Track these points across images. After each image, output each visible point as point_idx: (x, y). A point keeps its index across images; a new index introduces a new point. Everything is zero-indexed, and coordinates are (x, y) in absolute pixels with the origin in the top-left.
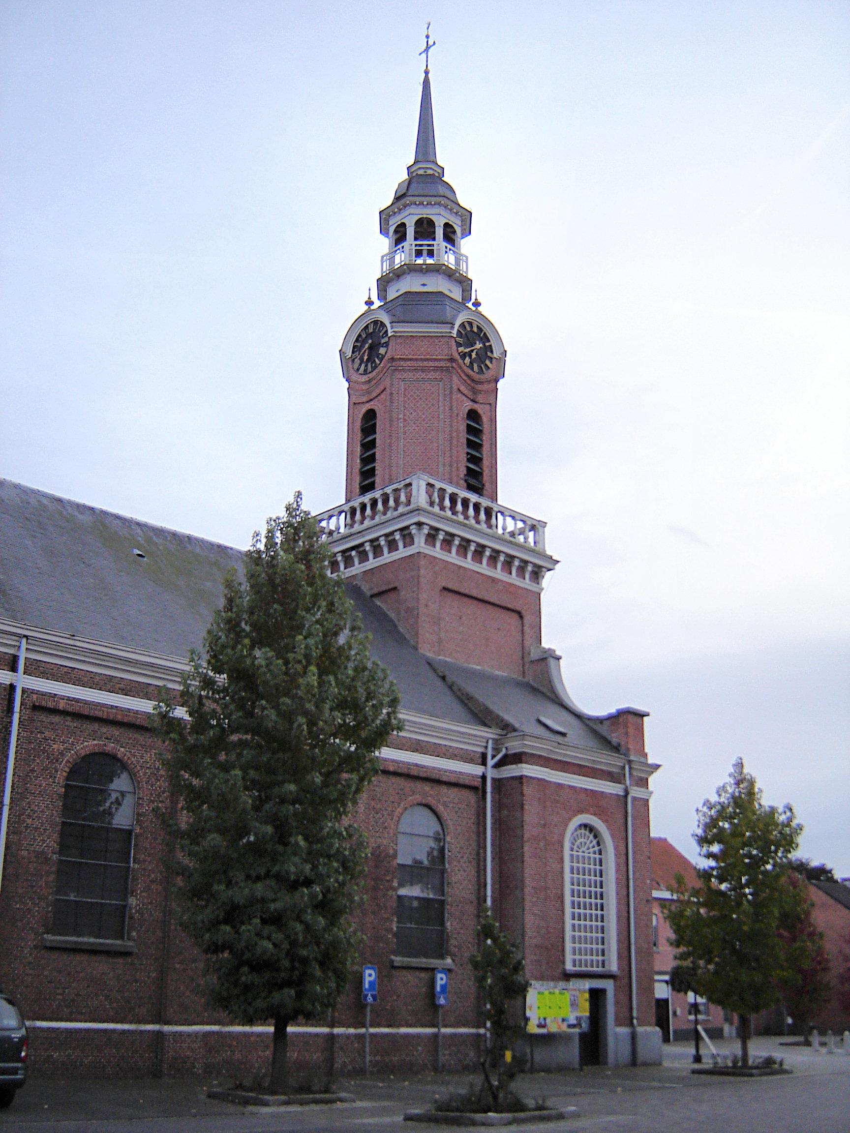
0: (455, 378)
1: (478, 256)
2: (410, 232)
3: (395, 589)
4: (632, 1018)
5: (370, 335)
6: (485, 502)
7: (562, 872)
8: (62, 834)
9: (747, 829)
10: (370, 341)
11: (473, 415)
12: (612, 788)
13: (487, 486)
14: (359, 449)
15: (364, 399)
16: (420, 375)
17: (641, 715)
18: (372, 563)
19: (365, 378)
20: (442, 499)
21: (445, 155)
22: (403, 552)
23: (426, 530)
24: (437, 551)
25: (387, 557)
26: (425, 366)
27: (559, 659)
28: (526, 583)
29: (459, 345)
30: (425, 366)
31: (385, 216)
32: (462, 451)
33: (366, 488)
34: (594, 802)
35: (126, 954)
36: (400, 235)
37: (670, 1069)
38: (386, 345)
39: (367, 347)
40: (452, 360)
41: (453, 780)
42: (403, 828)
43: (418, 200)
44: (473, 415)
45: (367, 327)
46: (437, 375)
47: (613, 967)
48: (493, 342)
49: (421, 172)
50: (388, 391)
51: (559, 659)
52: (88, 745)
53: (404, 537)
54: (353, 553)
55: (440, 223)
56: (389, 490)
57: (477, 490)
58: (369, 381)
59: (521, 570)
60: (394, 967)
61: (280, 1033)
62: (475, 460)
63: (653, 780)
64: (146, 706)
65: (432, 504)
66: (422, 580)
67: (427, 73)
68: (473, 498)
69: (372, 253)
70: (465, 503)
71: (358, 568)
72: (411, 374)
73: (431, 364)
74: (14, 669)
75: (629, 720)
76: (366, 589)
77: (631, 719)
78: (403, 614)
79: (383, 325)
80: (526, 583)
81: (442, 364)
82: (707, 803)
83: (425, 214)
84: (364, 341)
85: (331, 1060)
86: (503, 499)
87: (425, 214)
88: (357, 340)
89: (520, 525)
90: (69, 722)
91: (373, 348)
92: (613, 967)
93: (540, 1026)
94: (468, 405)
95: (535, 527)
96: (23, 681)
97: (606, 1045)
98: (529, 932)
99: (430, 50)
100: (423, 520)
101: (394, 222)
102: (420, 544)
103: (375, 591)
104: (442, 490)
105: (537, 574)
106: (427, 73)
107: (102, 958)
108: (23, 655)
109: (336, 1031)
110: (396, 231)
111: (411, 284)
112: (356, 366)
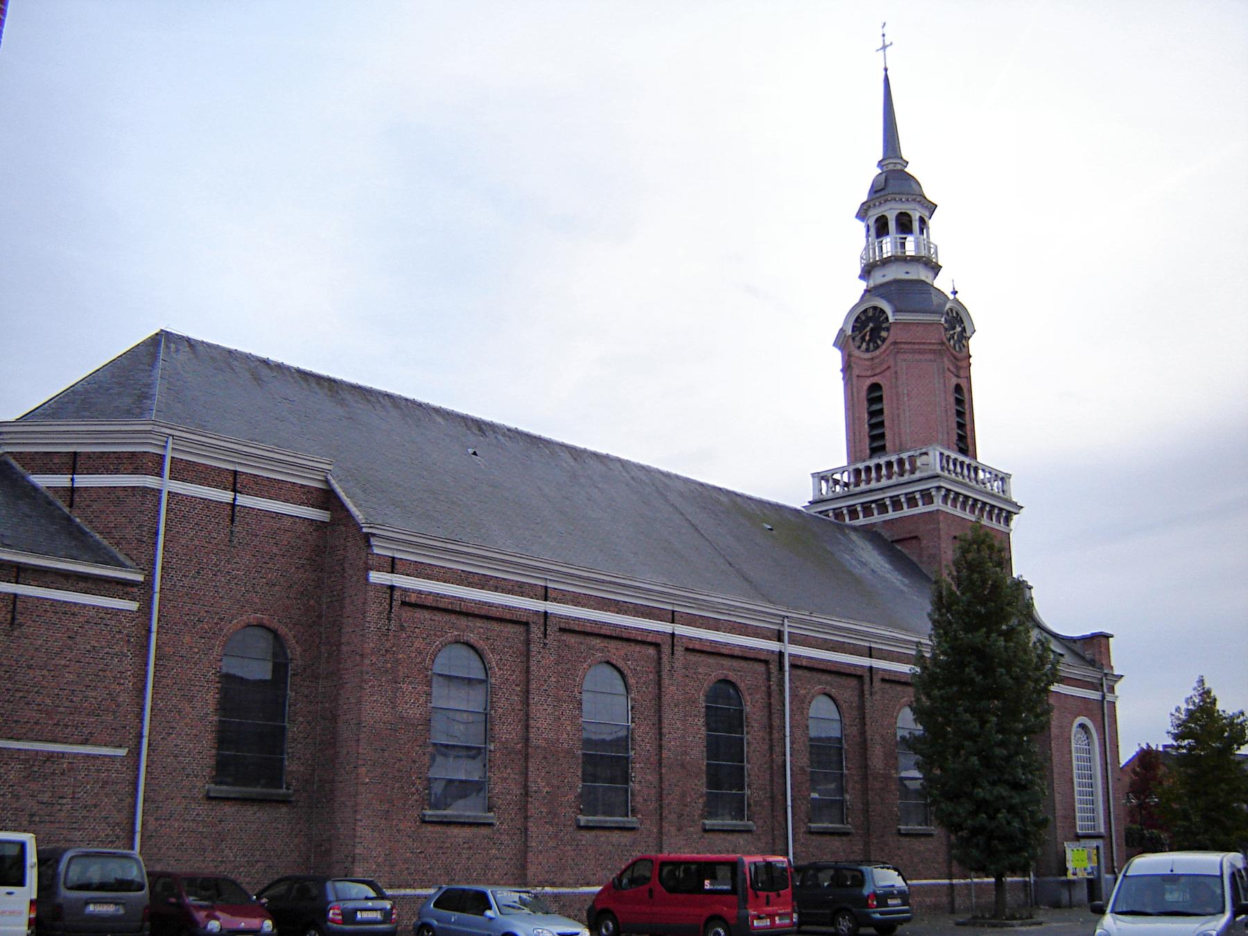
0: (945, 359)
1: (943, 233)
2: (892, 225)
3: (916, 537)
4: (1113, 867)
5: (869, 319)
6: (974, 464)
7: (1071, 761)
8: (811, 753)
9: (1204, 724)
10: (871, 325)
11: (958, 388)
12: (1094, 695)
13: (971, 448)
14: (866, 416)
15: (869, 373)
16: (917, 357)
17: (1107, 637)
18: (891, 515)
19: (868, 356)
20: (948, 462)
21: (907, 150)
22: (921, 509)
23: (943, 492)
24: (948, 508)
25: (907, 511)
26: (905, 344)
27: (1030, 588)
28: (1001, 527)
29: (946, 330)
30: (905, 344)
31: (862, 214)
32: (954, 419)
33: (876, 450)
34: (1085, 706)
35: (846, 834)
36: (881, 228)
37: (759, 928)
38: (888, 329)
39: (865, 330)
40: (943, 343)
41: (752, 656)
42: (812, 713)
43: (898, 197)
44: (958, 388)
45: (865, 311)
46: (931, 356)
47: (1102, 829)
48: (966, 324)
49: (891, 167)
50: (892, 370)
51: (1030, 588)
52: (721, 673)
53: (922, 496)
54: (873, 505)
55: (916, 216)
56: (905, 456)
57: (964, 451)
58: (872, 359)
59: (964, 504)
60: (705, 831)
61: (999, 884)
62: (961, 426)
63: (1118, 687)
64: (905, 668)
65: (942, 469)
66: (942, 533)
67: (886, 70)
68: (961, 458)
69: (854, 239)
70: (962, 463)
71: (877, 518)
72: (911, 356)
73: (926, 347)
74: (780, 639)
75: (1099, 641)
76: (886, 535)
77: (1103, 640)
78: (925, 558)
79: (882, 311)
80: (1001, 527)
81: (935, 347)
82: (1178, 709)
83: (896, 203)
84: (864, 325)
85: (952, 902)
86: (981, 458)
87: (896, 203)
88: (856, 321)
89: (988, 475)
90: (807, 674)
91: (875, 332)
92: (1102, 829)
93: (1074, 874)
94: (954, 381)
95: (1004, 478)
96: (791, 649)
97: (1100, 889)
98: (1058, 806)
99: (888, 49)
100: (942, 484)
101: (874, 214)
102: (938, 504)
103: (896, 538)
104: (948, 457)
105: (1008, 520)
106: (886, 70)
107: (836, 838)
108: (786, 630)
109: (955, 881)
110: (877, 220)
111: (895, 273)
112: (858, 344)
